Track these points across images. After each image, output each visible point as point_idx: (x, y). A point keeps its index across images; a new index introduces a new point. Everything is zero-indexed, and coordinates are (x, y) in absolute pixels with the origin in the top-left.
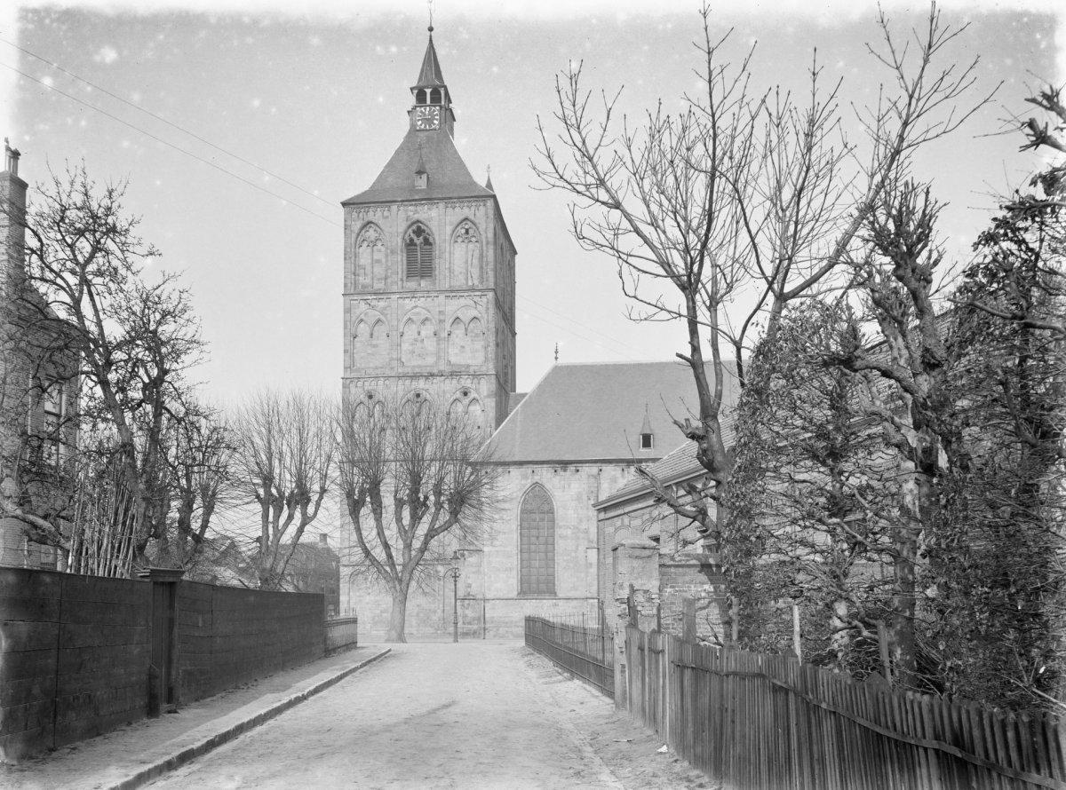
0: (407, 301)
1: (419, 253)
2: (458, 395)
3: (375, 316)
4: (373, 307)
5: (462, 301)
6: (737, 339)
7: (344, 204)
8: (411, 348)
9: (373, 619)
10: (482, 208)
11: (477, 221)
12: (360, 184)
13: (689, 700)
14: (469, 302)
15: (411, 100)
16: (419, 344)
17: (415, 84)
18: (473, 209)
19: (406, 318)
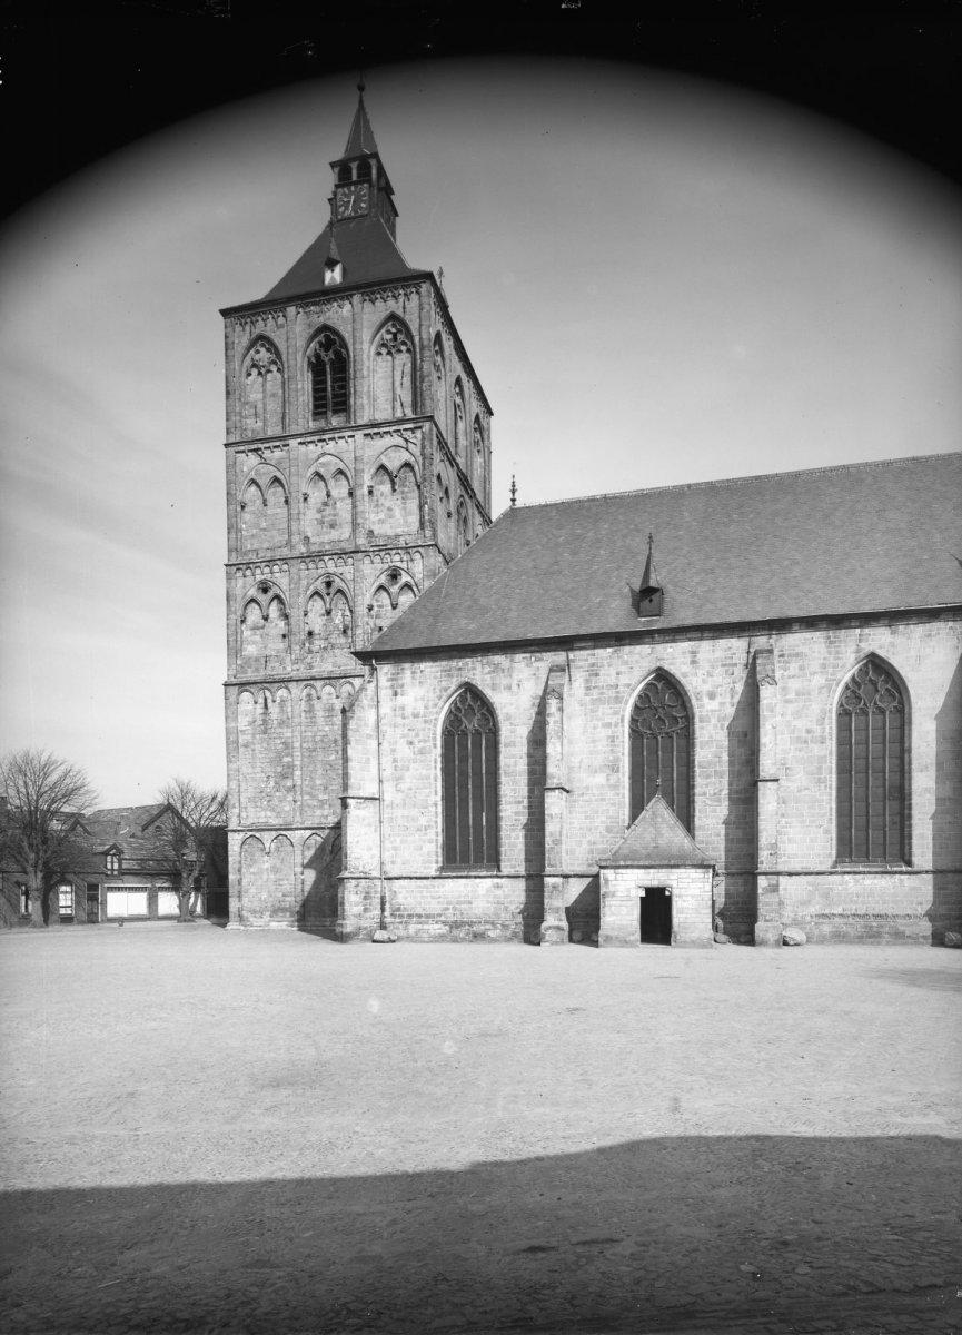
0: (311, 446)
5: (388, 441)
8: (319, 516)
10: (414, 297)
14: (398, 440)
15: (330, 178)
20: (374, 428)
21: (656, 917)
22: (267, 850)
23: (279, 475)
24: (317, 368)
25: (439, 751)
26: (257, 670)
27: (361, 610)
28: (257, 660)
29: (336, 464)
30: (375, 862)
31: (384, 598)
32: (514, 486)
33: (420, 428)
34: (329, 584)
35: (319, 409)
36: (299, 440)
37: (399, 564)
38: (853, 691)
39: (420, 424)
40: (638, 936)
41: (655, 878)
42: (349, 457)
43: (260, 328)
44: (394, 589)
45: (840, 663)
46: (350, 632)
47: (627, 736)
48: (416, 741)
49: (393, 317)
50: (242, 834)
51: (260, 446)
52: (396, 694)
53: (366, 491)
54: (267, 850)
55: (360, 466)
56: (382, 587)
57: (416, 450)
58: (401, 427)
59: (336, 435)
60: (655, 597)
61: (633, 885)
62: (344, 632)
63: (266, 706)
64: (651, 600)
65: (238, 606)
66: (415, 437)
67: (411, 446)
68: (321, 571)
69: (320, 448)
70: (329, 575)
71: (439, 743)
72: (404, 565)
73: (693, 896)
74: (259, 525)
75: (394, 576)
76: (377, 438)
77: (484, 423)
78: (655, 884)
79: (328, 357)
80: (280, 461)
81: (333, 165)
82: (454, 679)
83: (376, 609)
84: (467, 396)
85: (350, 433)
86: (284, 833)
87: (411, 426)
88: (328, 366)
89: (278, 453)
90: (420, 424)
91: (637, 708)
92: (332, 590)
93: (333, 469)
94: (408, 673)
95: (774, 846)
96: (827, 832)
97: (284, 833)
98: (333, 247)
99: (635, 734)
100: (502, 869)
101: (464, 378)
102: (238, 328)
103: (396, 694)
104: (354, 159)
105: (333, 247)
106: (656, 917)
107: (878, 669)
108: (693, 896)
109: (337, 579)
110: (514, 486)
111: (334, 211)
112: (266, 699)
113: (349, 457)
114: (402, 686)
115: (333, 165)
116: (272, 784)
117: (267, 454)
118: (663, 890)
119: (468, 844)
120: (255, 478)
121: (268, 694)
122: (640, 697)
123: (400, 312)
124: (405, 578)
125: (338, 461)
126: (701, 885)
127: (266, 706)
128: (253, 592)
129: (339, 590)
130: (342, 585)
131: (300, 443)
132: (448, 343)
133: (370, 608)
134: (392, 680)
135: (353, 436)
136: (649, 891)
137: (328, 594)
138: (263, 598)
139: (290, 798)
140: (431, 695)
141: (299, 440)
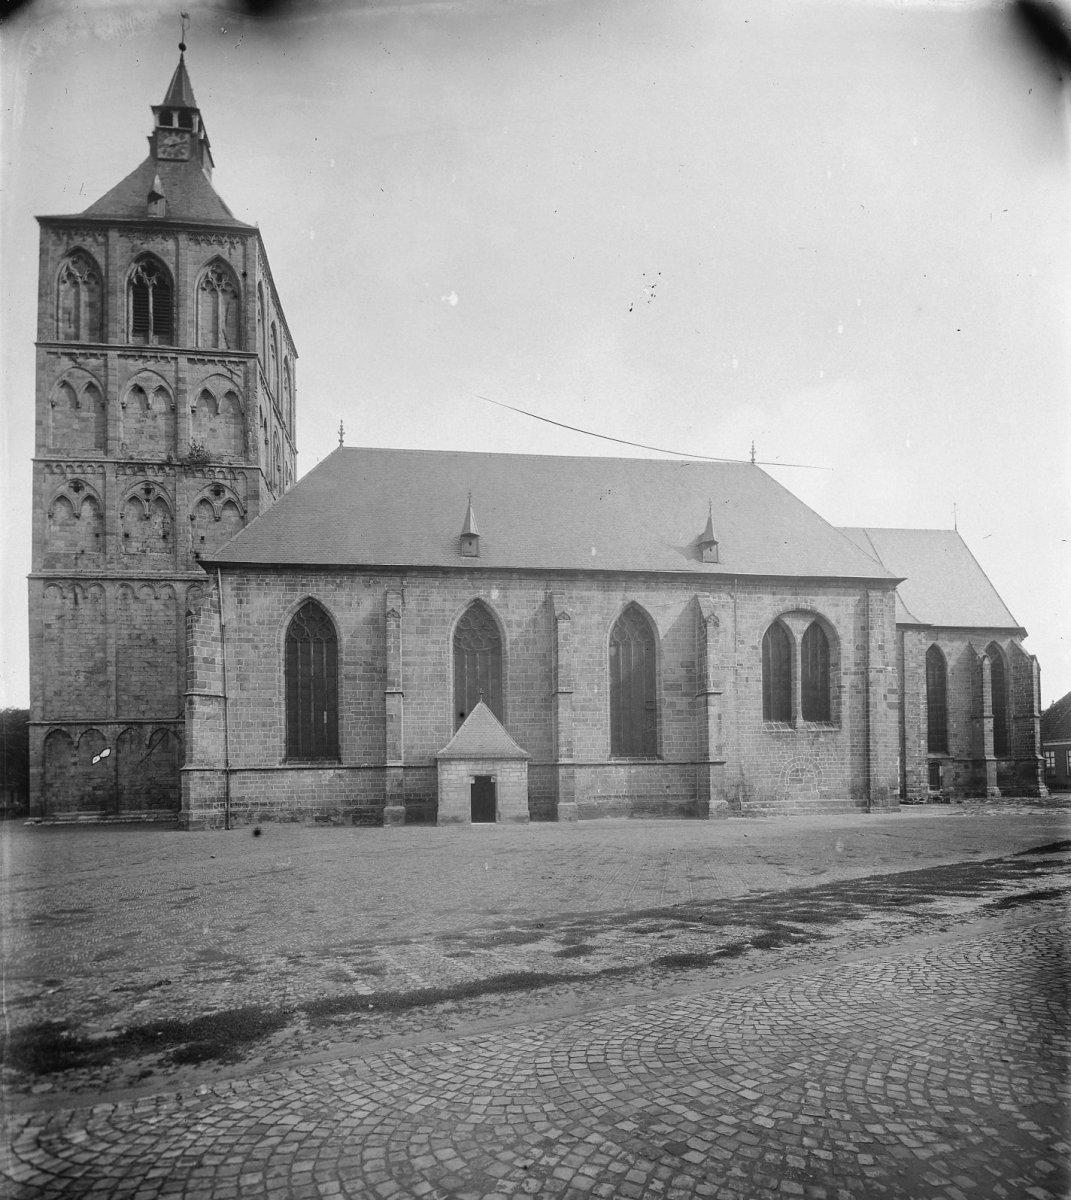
0: (131, 361)
1: (157, 308)
2: (207, 493)
3: (84, 377)
4: (79, 366)
5: (211, 369)
6: (317, 1169)
7: (48, 223)
8: (138, 426)
9: (82, 798)
10: (240, 248)
11: (232, 263)
12: (75, 205)
13: (917, 815)
14: (220, 369)
15: (150, 123)
16: (149, 422)
17: (159, 101)
18: (227, 246)
19: (199, 497)
20: (198, 357)
21: (484, 800)
22: (76, 744)
23: (94, 380)
24: (138, 289)
25: (282, 655)
26: (66, 566)
27: (183, 517)
28: (67, 556)
29: (157, 382)
30: (221, 755)
31: (205, 512)
32: (342, 429)
33: (245, 362)
34: (148, 491)
35: (140, 328)
36: (119, 353)
37: (221, 481)
38: (619, 626)
39: (245, 360)
40: (469, 813)
41: (483, 769)
42: (170, 376)
43: (77, 241)
44: (218, 503)
45: (612, 607)
46: (170, 538)
47: (451, 651)
48: (261, 645)
49: (218, 261)
50: (46, 728)
51: (75, 351)
52: (241, 602)
53: (188, 410)
54: (76, 744)
55: (181, 386)
56: (204, 501)
57: (240, 381)
58: (227, 359)
59: (159, 355)
60: (474, 542)
61: (464, 773)
62: (164, 537)
63: (76, 603)
64: (470, 544)
65: (47, 502)
66: (240, 370)
67: (235, 378)
68: (142, 479)
69: (140, 363)
70: (148, 483)
71: (283, 649)
72: (227, 483)
73: (513, 784)
74: (70, 426)
75: (218, 490)
76: (199, 366)
77: (290, 364)
78: (484, 773)
79: (151, 282)
80: (97, 368)
81: (154, 109)
82: (299, 593)
83: (198, 519)
84: (278, 338)
85: (174, 355)
86: (94, 727)
87: (236, 360)
88: (150, 290)
89: (93, 361)
90: (245, 360)
91: (458, 630)
92: (151, 497)
93: (155, 385)
94: (253, 585)
95: (569, 743)
96: (604, 733)
97: (94, 727)
98: (157, 181)
99: (458, 651)
100: (343, 761)
101: (277, 324)
102: (53, 237)
103: (241, 602)
104: (175, 109)
105: (157, 181)
106: (484, 800)
107: (479, 608)
108: (513, 784)
109: (157, 488)
110: (342, 429)
111: (153, 151)
112: (76, 595)
113: (170, 376)
114: (247, 595)
115: (154, 109)
116: (82, 679)
117: (81, 360)
118: (488, 778)
119: (312, 736)
120: (67, 379)
121: (78, 590)
122: (461, 620)
123: (226, 256)
124: (228, 495)
125: (160, 378)
126: (519, 774)
127: (76, 603)
128: (64, 489)
129: (159, 499)
130: (162, 494)
131: (119, 356)
132: (266, 291)
133: (192, 519)
134: (238, 589)
135: (176, 359)
136: (477, 778)
137: (148, 500)
138: (73, 496)
139: (103, 692)
140: (276, 605)
141: (119, 353)
